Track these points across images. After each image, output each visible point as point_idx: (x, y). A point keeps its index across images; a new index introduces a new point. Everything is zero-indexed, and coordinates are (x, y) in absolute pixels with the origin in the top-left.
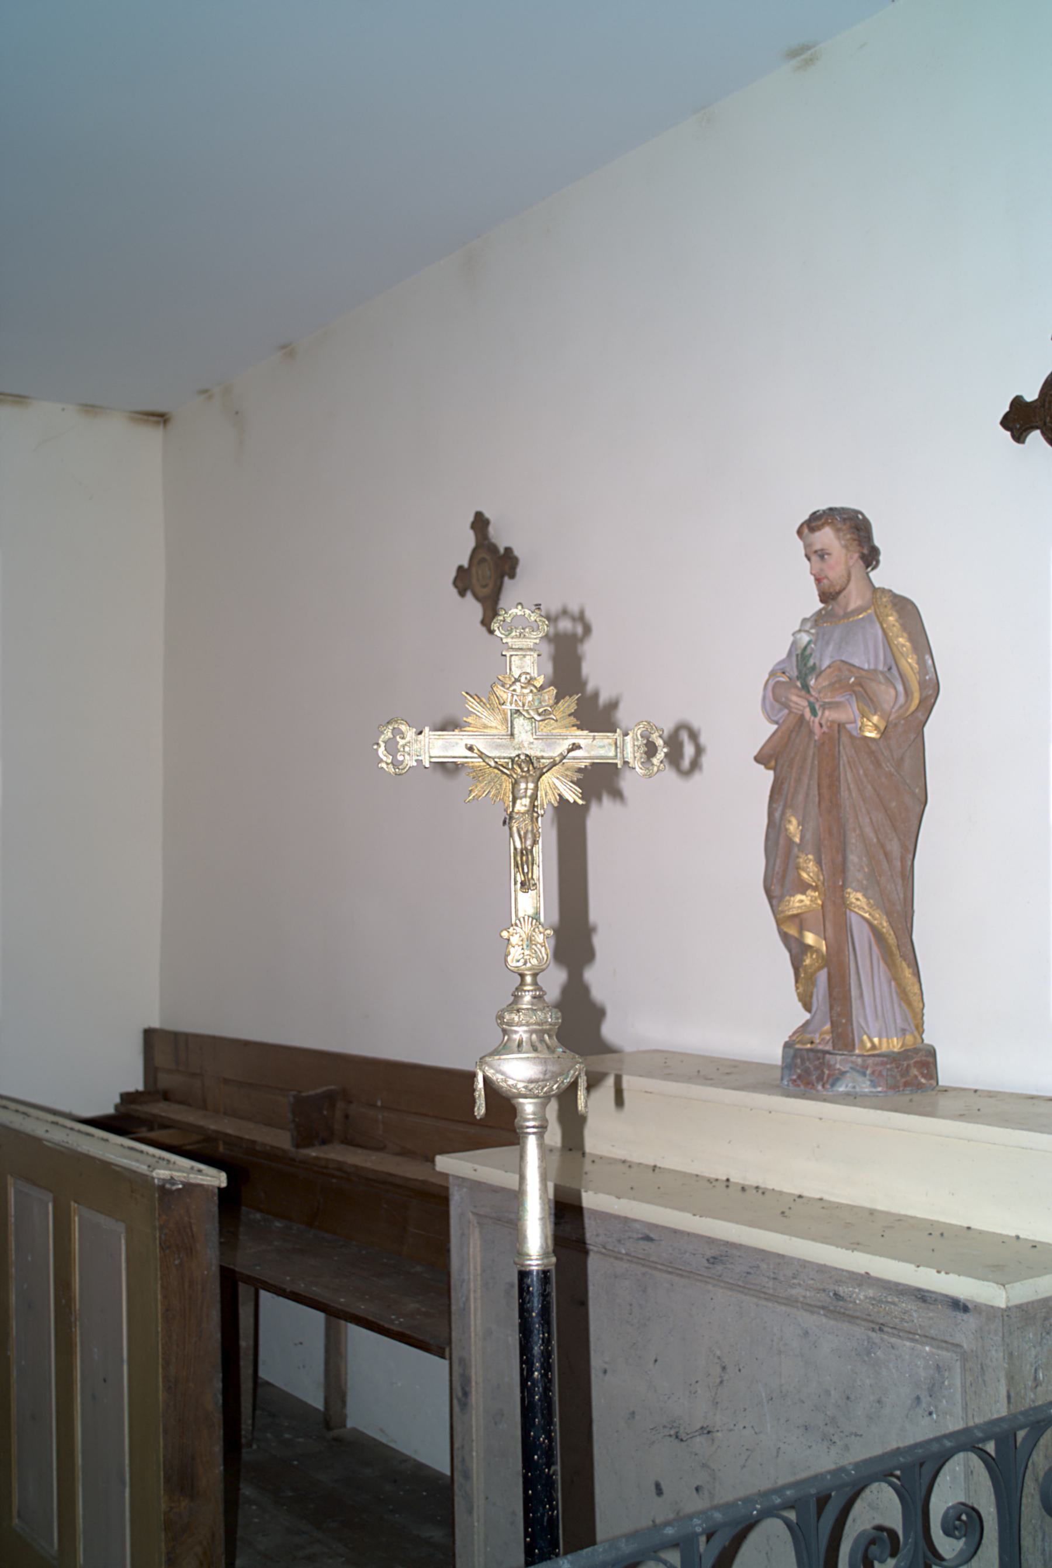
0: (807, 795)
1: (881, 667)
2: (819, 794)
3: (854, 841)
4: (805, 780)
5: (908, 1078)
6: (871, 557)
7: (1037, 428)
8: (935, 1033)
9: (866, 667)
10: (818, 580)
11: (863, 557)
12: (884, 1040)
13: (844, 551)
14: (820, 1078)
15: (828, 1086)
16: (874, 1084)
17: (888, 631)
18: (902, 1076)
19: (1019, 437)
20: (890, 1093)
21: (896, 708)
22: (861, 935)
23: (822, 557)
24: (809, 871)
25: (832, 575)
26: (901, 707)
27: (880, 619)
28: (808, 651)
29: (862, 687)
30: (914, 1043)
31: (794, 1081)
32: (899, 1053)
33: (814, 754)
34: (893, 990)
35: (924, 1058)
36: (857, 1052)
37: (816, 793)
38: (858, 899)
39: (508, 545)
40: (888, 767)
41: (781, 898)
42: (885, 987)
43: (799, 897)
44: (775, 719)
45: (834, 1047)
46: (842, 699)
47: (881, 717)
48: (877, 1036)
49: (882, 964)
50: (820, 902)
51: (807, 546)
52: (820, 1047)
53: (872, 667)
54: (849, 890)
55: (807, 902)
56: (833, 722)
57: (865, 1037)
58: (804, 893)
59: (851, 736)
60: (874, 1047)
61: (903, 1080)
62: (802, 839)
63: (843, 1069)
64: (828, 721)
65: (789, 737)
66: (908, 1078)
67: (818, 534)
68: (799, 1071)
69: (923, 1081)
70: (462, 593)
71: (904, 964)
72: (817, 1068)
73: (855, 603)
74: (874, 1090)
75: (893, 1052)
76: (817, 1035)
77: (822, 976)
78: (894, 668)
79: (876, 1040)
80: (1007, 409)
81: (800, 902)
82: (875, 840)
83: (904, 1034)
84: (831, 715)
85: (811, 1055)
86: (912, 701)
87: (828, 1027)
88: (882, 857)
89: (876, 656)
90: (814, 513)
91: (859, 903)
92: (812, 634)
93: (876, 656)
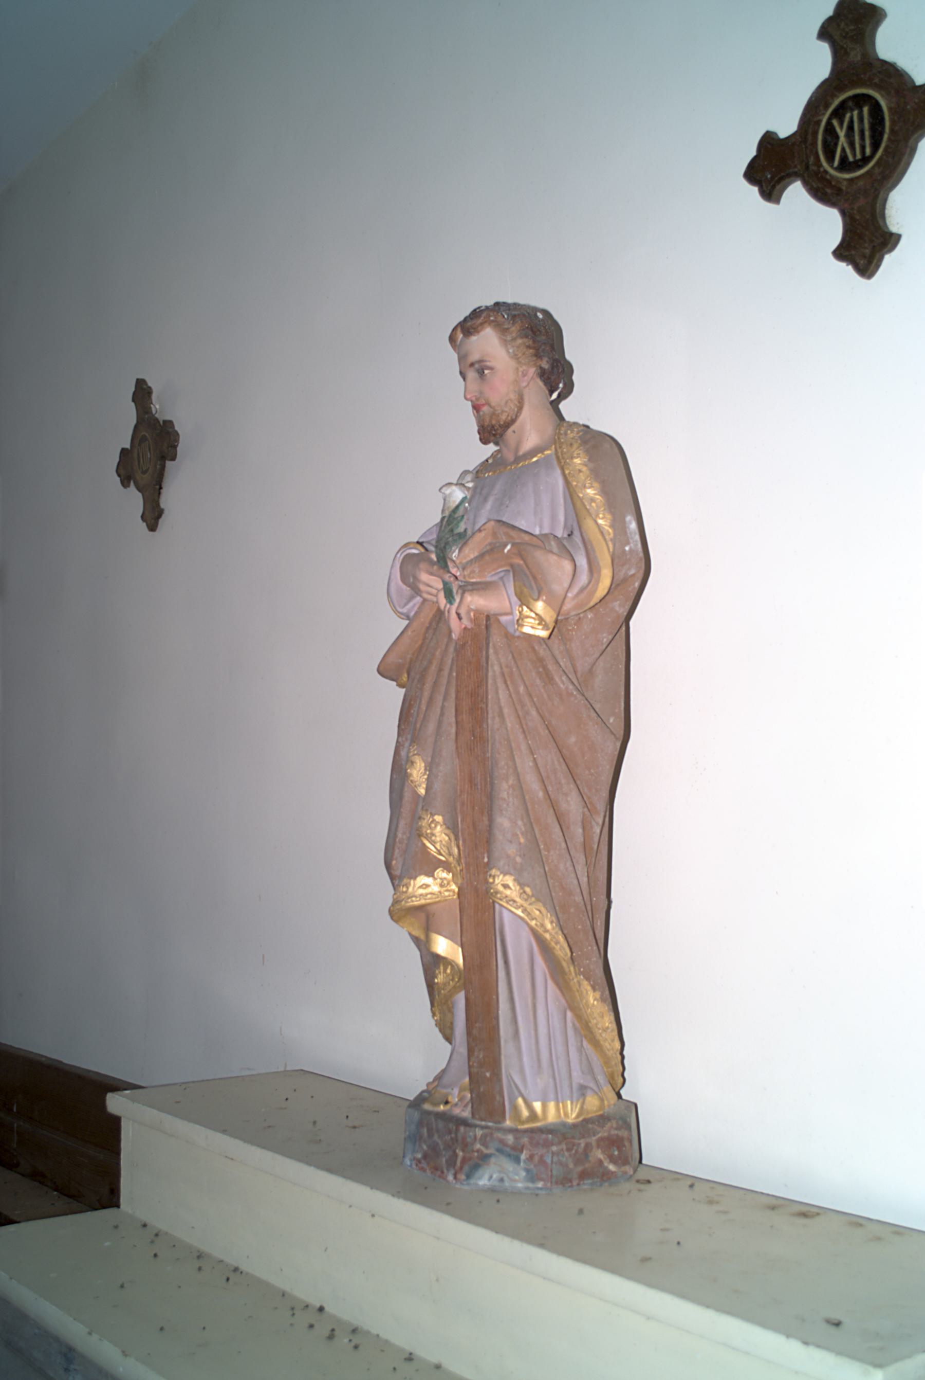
0: (440, 724)
1: (560, 533)
2: (457, 723)
3: (505, 795)
4: (439, 698)
5: (587, 1165)
6: (558, 376)
7: (796, 175)
8: (652, 1084)
9: (537, 532)
10: (476, 408)
11: (543, 374)
12: (552, 1106)
13: (513, 364)
14: (451, 1163)
15: (462, 1177)
16: (532, 1177)
17: (570, 479)
18: (577, 1162)
19: (771, 193)
20: (558, 1190)
21: (575, 590)
22: (517, 944)
23: (481, 372)
24: (438, 838)
25: (495, 399)
26: (582, 590)
27: (562, 462)
28: (461, 511)
29: (523, 559)
30: (602, 1107)
31: (419, 1161)
32: (574, 1126)
33: (453, 660)
34: (569, 1024)
35: (614, 1132)
36: (508, 1123)
37: (453, 720)
38: (506, 886)
39: (168, 418)
40: (562, 683)
41: (401, 878)
42: (556, 1023)
43: (423, 880)
44: (404, 610)
45: (473, 1114)
46: (495, 578)
47: (548, 603)
48: (543, 1100)
49: (550, 982)
50: (454, 887)
51: (462, 359)
52: (457, 1111)
53: (546, 531)
54: (494, 872)
55: (435, 888)
56: (477, 612)
57: (520, 1101)
58: (430, 874)
59: (508, 636)
60: (533, 1116)
61: (580, 1168)
62: (427, 790)
63: (485, 1151)
64: (469, 610)
65: (425, 638)
66: (587, 1165)
67: (474, 338)
68: (425, 1147)
69: (612, 1167)
70: (125, 482)
71: (586, 985)
72: (448, 1147)
73: (531, 440)
74: (531, 1185)
75: (564, 1124)
76: (456, 1091)
77: (460, 1000)
78: (577, 533)
79: (537, 1106)
80: (754, 153)
81: (429, 887)
82: (541, 794)
83: (583, 1095)
84: (475, 601)
85: (441, 1124)
86: (598, 582)
87: (467, 1080)
88: (551, 819)
89: (554, 518)
90: (475, 310)
91: (508, 892)
92: (468, 489)
93: (554, 518)
